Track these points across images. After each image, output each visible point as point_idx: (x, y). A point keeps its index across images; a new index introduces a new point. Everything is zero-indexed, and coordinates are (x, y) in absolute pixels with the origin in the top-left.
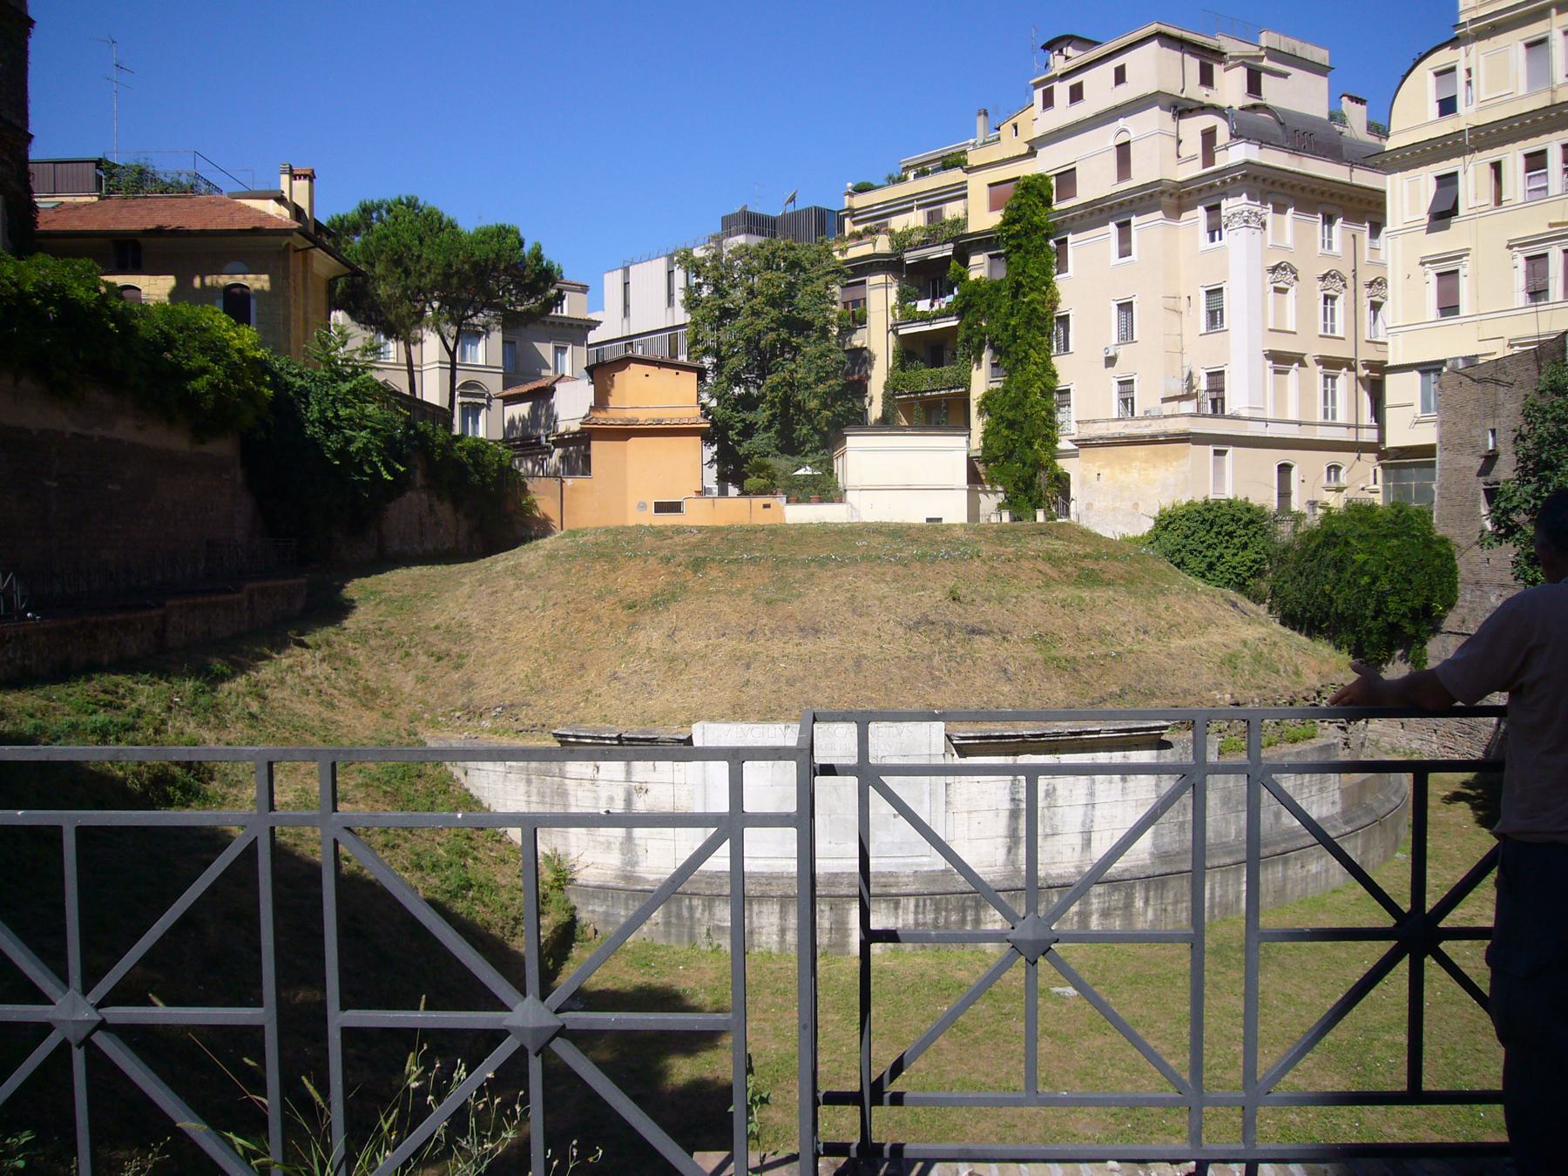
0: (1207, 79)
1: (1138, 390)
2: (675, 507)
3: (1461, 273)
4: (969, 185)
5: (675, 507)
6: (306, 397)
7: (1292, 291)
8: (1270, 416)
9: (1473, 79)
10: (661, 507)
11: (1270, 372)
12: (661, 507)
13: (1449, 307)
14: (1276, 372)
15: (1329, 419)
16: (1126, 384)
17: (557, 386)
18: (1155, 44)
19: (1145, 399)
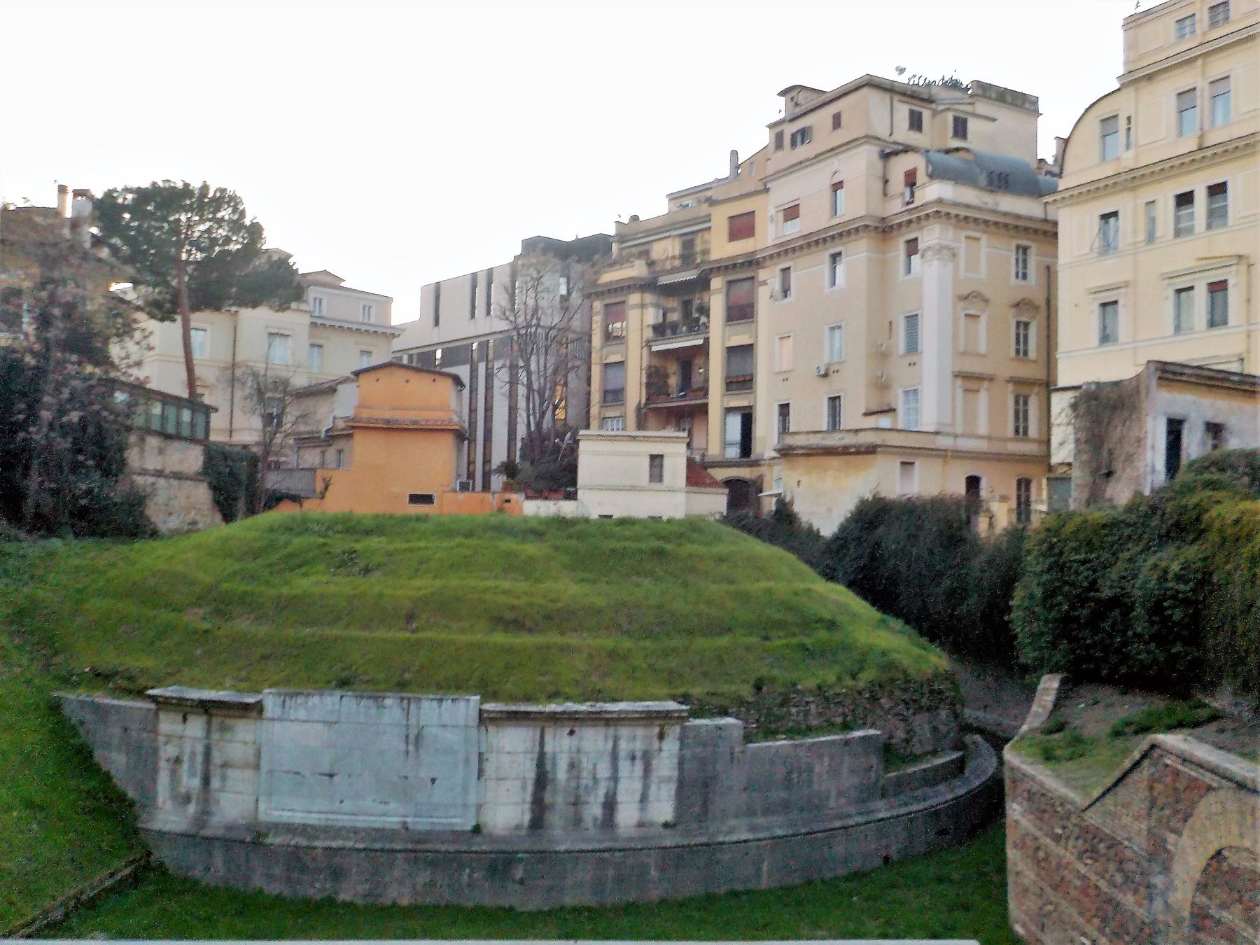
0: (916, 123)
1: (844, 405)
2: (427, 499)
3: (1121, 303)
4: (713, 217)
5: (427, 499)
6: (1207, 916)
7: (983, 320)
8: (959, 430)
9: (1132, 125)
10: (415, 499)
11: (960, 392)
12: (415, 499)
13: (1106, 337)
14: (966, 390)
15: (953, 425)
16: (834, 401)
17: (340, 387)
18: (865, 91)
19: (851, 417)
